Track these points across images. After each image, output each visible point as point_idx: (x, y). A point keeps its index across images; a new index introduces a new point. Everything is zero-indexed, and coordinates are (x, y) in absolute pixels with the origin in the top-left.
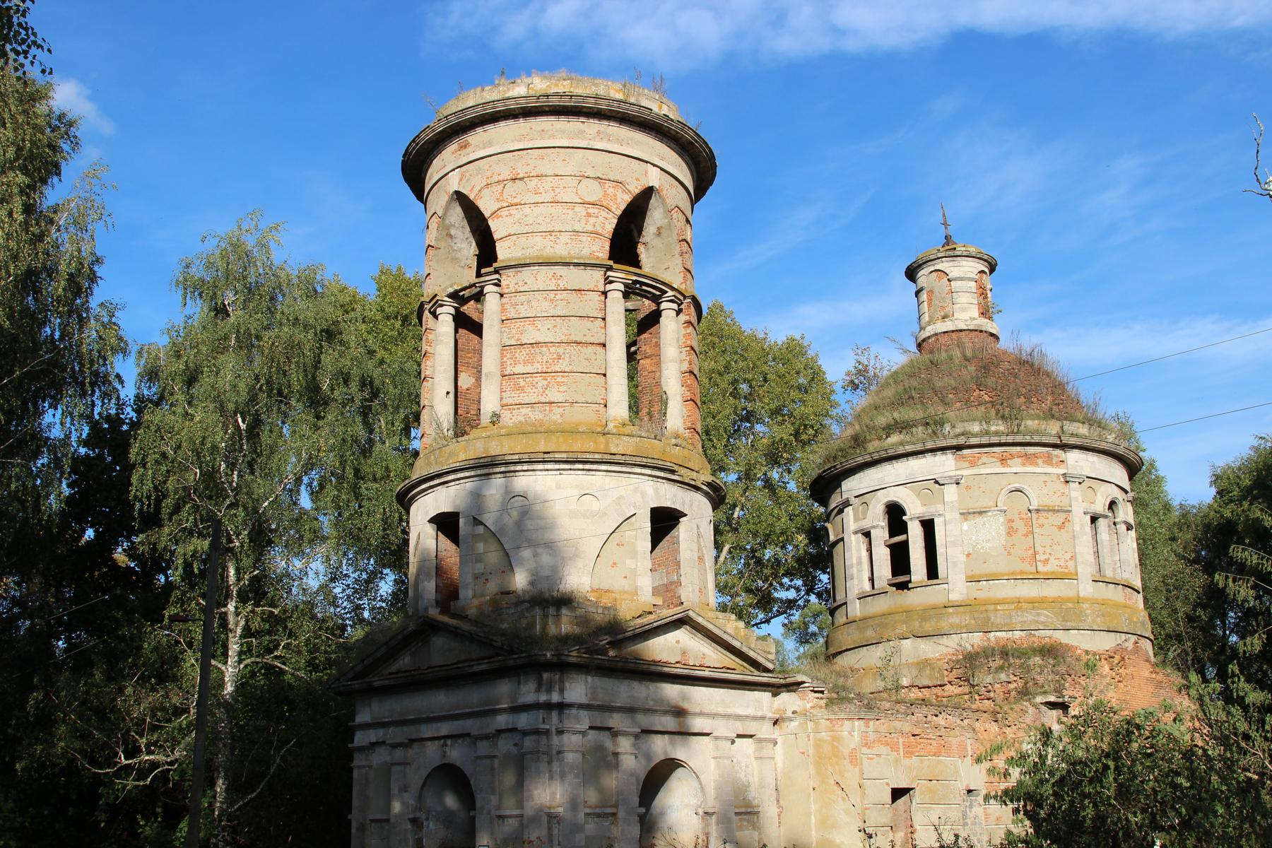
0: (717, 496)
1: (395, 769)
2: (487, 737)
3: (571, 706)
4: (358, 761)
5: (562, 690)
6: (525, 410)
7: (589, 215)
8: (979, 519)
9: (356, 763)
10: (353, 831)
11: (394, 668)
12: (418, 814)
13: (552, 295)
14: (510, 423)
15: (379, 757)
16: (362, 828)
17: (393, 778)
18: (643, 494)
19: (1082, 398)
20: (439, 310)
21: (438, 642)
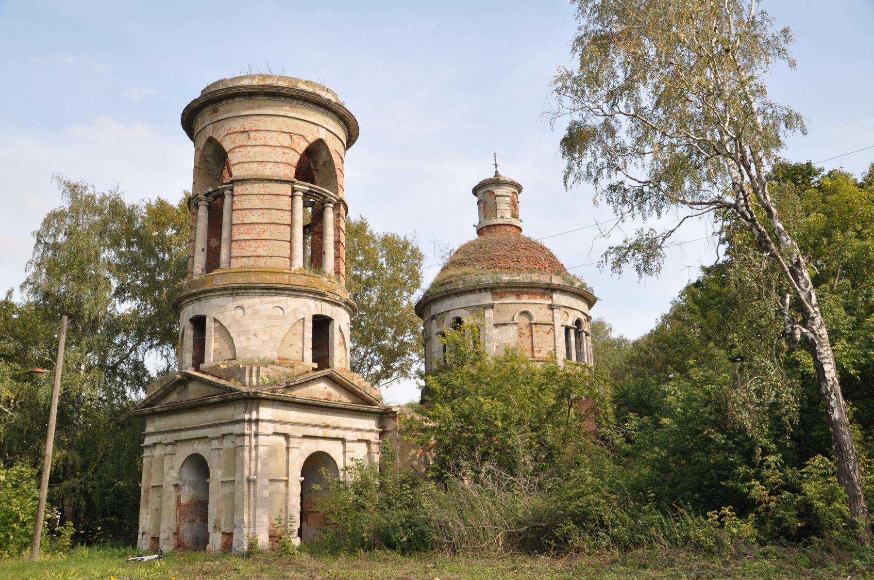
0: (351, 309)
1: (166, 457)
2: (217, 438)
3: (263, 421)
4: (147, 453)
5: (258, 412)
6: (244, 260)
7: (284, 153)
8: (503, 328)
9: (145, 454)
10: (142, 492)
11: (168, 402)
12: (178, 482)
13: (262, 197)
14: (236, 266)
15: (158, 452)
16: (147, 491)
17: (165, 462)
18: (309, 307)
19: (710, 263)
20: (200, 203)
21: (192, 386)
